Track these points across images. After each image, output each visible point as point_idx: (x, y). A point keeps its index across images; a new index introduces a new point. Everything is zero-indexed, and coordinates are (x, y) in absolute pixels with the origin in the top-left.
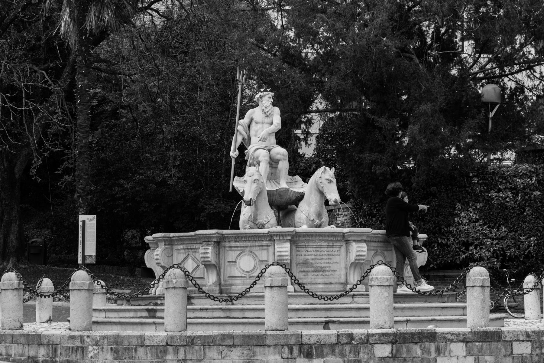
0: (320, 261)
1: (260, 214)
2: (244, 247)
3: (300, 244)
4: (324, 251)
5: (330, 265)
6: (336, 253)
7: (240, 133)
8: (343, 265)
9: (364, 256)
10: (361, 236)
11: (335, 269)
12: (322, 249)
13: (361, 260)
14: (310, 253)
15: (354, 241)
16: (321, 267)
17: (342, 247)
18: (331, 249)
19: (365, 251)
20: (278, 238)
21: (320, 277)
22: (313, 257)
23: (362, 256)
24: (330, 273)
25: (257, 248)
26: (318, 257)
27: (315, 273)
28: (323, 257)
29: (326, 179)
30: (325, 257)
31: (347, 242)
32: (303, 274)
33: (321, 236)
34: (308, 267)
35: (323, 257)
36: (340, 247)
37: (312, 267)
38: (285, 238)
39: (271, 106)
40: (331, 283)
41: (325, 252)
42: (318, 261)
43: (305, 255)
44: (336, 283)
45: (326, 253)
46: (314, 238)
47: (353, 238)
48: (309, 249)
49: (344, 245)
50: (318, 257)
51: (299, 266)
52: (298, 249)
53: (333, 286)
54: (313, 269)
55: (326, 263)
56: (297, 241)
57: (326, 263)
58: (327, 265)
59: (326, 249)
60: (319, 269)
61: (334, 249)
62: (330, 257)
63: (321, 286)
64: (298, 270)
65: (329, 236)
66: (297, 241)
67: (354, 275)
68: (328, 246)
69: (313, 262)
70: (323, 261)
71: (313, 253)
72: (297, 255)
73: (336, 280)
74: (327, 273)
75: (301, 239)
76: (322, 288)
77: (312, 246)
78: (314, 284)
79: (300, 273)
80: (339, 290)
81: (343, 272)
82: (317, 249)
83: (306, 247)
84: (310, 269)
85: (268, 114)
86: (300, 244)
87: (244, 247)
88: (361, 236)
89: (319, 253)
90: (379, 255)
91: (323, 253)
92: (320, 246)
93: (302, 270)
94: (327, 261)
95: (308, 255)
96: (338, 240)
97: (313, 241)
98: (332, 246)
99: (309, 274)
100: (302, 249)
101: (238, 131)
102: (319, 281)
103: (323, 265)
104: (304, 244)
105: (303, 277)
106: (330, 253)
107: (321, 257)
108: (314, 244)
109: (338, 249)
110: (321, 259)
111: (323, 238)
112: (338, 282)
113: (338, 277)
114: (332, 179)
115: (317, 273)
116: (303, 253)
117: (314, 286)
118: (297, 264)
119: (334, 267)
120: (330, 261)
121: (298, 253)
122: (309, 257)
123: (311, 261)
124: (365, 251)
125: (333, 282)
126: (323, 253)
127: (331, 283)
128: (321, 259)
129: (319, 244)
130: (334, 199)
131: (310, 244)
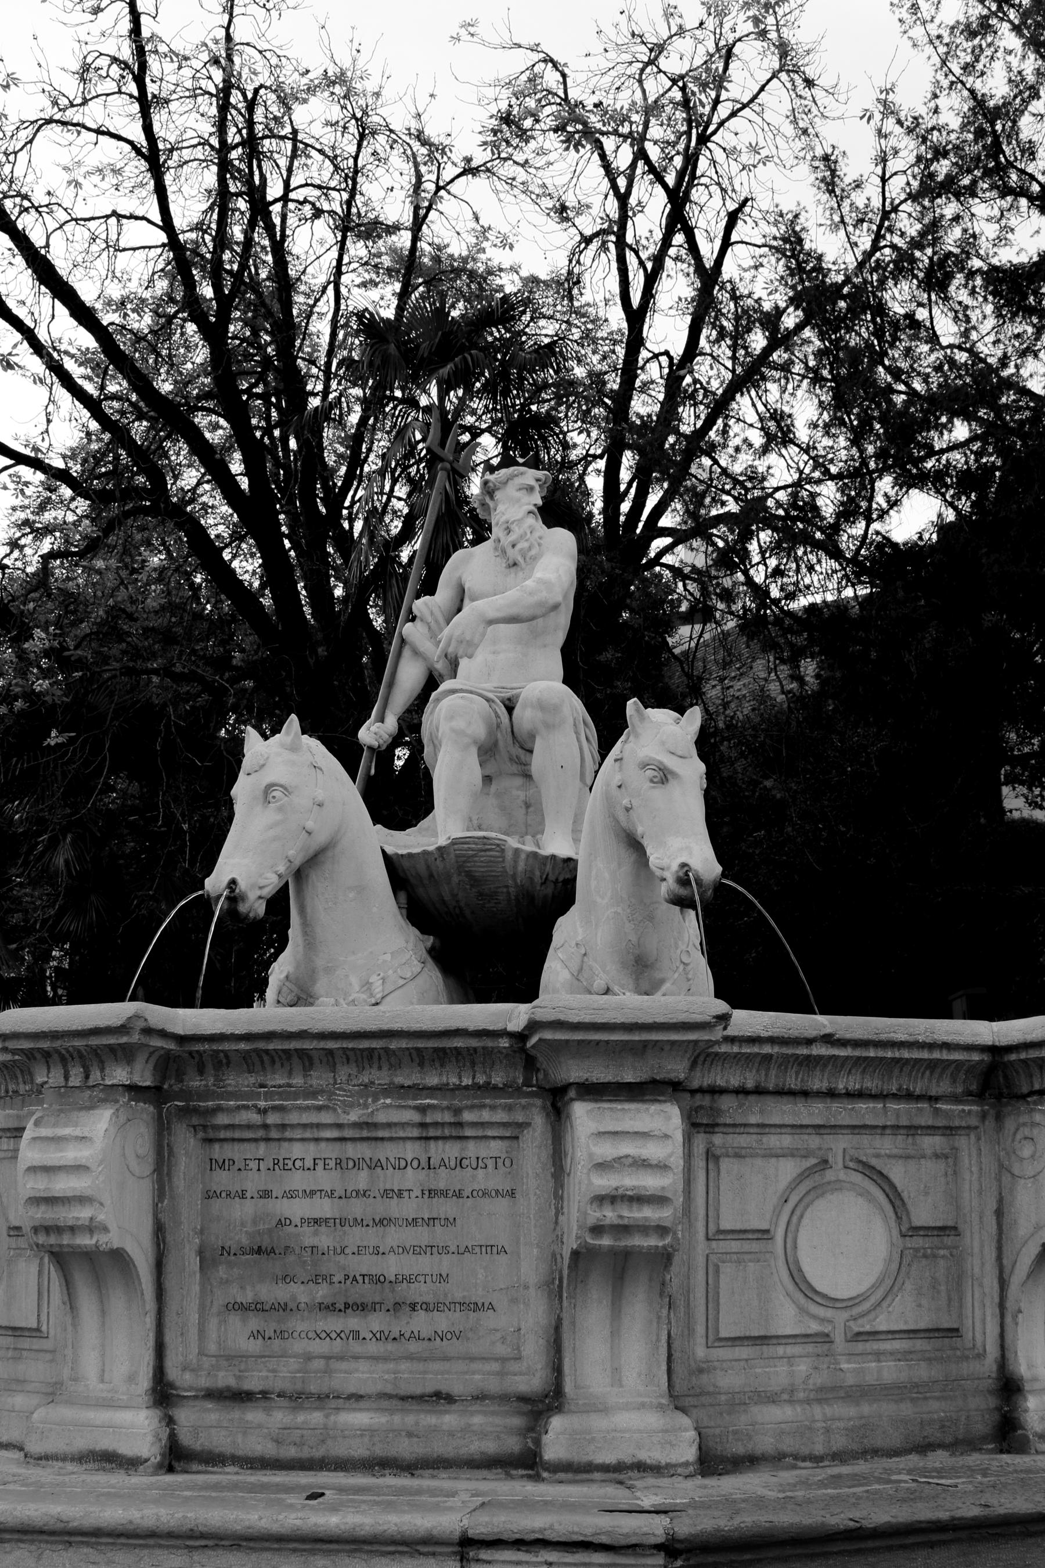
0: (370, 1237)
1: (328, 970)
2: (818, 1129)
3: (222, 1119)
4: (401, 1165)
5: (445, 1264)
6: (482, 1179)
7: (416, 653)
8: (530, 1268)
9: (658, 1200)
10: (642, 1049)
11: (478, 1296)
12: (388, 1152)
13: (644, 1229)
14: (298, 1180)
15: (593, 1091)
16: (378, 1280)
17: (527, 1135)
18: (451, 1151)
19: (662, 1167)
20: (56, 1077)
21: (373, 1348)
22: (324, 1208)
23: (638, 1199)
24: (442, 1321)
25: (902, 1131)
26: (357, 1208)
27: (334, 1323)
28: (395, 1208)
29: (644, 766)
30: (408, 1208)
31: (557, 1100)
32: (254, 1322)
33: (368, 1058)
34: (287, 1278)
35: (395, 1208)
36: (514, 1133)
37: (316, 1279)
38: (95, 1076)
39: (539, 524)
40: (441, 1398)
41: (404, 1170)
42: (355, 1236)
43: (266, 1194)
44: (480, 1397)
45: (411, 1178)
46: (319, 1078)
47: (600, 1073)
48: (297, 1150)
49: (539, 1120)
50: (357, 1208)
51: (222, 1272)
52: (218, 1152)
53: (450, 1419)
54: (322, 1292)
55: (418, 1250)
56: (205, 1094)
57: (418, 1250)
58: (424, 1264)
59: (411, 1151)
60: (365, 1292)
61: (472, 1149)
62: (445, 1208)
63: (359, 1418)
64: (220, 1298)
65: (421, 1058)
66: (205, 1094)
67: (615, 1333)
68: (426, 1133)
69: (324, 1239)
70: (394, 1236)
71: (325, 1179)
72: (209, 1195)
73: (481, 1378)
74: (421, 1322)
75: (234, 1080)
76: (370, 1432)
77: (312, 1134)
78: (322, 1399)
79: (234, 1320)
80: (490, 1447)
81: (534, 1315)
82: (352, 1151)
83: (265, 1134)
84: (301, 1293)
85: (513, 554)
86: (222, 1119)
87: (818, 1129)
88: (642, 1049)
89: (361, 1179)
90: (837, 1186)
91: (393, 1180)
92: (369, 1132)
93: (247, 1296)
94: (421, 1236)
95: (290, 1195)
96: (488, 1088)
97: (314, 1094)
98: (457, 1132)
99: (298, 1324)
100: (249, 1151)
101: (403, 641)
102: (362, 1376)
103: (392, 1266)
104: (255, 1118)
105: (255, 1346)
106: (442, 1180)
107: (380, 1208)
108: (326, 1118)
109: (496, 1148)
110: (383, 1222)
111: (380, 1077)
112: (493, 1386)
113: (501, 1350)
114: (671, 762)
115: (353, 1322)
116: (253, 1182)
117: (316, 1417)
118: (209, 1258)
119: (472, 1278)
120: (440, 1235)
121: (222, 1179)
122: (298, 1209)
123: (308, 1237)
124: (662, 1167)
125: (456, 1388)
126: (393, 1180)
127: (441, 1398)
128: (383, 1222)
129: (354, 1116)
130: (675, 867)
131: (293, 1118)
